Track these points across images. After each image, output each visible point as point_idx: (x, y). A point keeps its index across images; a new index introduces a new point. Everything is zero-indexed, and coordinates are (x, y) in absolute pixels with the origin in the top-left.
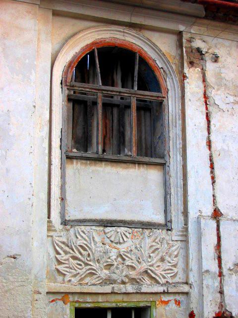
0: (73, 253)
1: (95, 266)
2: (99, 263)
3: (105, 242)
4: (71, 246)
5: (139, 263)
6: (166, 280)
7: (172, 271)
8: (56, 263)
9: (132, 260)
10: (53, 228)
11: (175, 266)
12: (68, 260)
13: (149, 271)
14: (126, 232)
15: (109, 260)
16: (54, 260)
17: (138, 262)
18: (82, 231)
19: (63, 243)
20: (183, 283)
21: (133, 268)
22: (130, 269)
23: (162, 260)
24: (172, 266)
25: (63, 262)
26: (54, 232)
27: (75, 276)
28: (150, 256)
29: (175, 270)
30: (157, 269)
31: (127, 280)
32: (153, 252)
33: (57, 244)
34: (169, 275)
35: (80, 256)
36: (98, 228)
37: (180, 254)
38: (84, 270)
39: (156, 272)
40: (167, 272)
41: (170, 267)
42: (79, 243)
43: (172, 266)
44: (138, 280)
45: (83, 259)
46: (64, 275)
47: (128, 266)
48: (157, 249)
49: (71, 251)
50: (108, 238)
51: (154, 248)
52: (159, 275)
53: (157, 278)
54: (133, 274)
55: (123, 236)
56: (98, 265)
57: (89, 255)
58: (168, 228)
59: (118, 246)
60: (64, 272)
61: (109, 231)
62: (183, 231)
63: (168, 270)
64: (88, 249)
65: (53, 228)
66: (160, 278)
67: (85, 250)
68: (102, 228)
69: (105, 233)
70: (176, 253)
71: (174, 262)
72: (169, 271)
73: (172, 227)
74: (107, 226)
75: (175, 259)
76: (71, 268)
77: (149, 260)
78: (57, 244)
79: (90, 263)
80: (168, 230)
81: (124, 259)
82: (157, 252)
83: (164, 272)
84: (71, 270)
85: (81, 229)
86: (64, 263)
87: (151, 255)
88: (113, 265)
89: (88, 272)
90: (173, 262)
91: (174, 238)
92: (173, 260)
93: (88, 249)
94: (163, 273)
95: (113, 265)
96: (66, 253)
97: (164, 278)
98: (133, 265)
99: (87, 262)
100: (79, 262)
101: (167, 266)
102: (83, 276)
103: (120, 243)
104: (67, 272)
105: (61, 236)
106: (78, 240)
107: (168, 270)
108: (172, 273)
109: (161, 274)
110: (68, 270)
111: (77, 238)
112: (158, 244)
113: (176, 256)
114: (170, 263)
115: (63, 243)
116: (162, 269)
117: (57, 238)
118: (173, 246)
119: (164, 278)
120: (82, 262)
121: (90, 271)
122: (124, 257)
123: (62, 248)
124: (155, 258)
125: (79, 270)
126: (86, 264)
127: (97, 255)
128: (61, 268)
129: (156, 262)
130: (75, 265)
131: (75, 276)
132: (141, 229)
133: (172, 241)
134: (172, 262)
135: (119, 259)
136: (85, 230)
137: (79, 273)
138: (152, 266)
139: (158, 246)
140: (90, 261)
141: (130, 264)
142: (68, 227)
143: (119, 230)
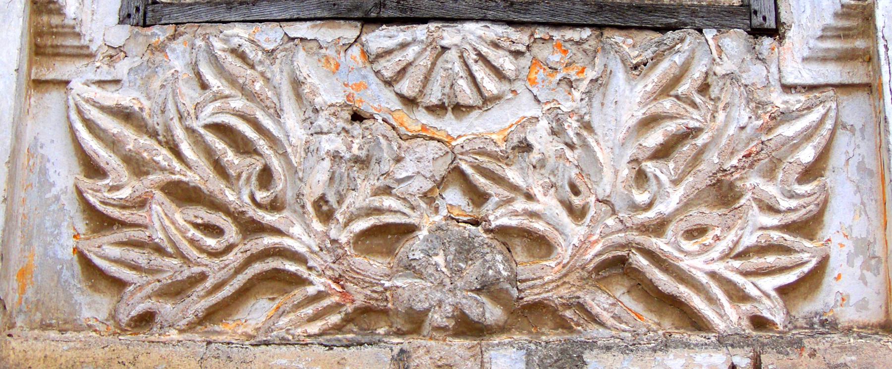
0: (177, 165)
1: (300, 234)
2: (327, 216)
3: (365, 107)
4: (168, 129)
5: (577, 214)
6: (746, 307)
7: (785, 260)
8: (82, 226)
9: (529, 197)
10: (71, 42)
11: (807, 227)
12: (142, 203)
13: (640, 261)
14: (496, 45)
15: (388, 202)
16: (72, 207)
17: (570, 209)
18: (233, 51)
19: (125, 115)
20: (439, 56)
21: (540, 244)
22: (520, 255)
23: (724, 193)
24: (786, 228)
25: (115, 213)
26: (80, 64)
27: (177, 291)
28: (641, 177)
29: (807, 253)
30: (689, 246)
31: (493, 313)
32: (663, 153)
33: (90, 124)
34: (770, 283)
35: (214, 185)
36: (327, 34)
37: (837, 159)
38: (234, 258)
39: (686, 264)
40: (756, 262)
41: (776, 235)
42: (208, 115)
43: (786, 228)
44: (568, 314)
45: (230, 196)
46: (119, 284)
47: (503, 232)
48: (690, 133)
49: (163, 156)
50: (389, 83)
51: (672, 127)
52: (704, 279)
53: (697, 302)
54: (542, 278)
55: (480, 72)
56: (317, 226)
57: (266, 177)
58: (757, 21)
59: (449, 125)
60: (114, 270)
61: (389, 44)
62: (844, 34)
63: (762, 250)
64: (262, 144)
65: (71, 42)
66: (711, 300)
67: (243, 146)
68: (349, 32)
69: (372, 58)
70: (807, 155)
71: (794, 207)
72: (771, 259)
73: (784, 17)
74: (380, 21)
75: (801, 189)
76: (159, 250)
77: (642, 198)
78: (90, 124)
79: (268, 218)
80: (757, 32)
81: (479, 197)
82: (686, 149)
83: (737, 264)
84: (158, 260)
85: (226, 40)
86: (123, 224)
87: (650, 167)
88: (408, 230)
89: (258, 267)
90: (793, 203)
91: (798, 72)
92: (792, 196)
93: (262, 144)
94: (729, 270)
95: (408, 230)
96: (138, 166)
97: (738, 295)
98: (539, 226)
99: (253, 212)
100: (205, 215)
101: (754, 226)
102: (227, 291)
103: (460, 109)
104: (136, 268)
105: (117, 82)
106: (208, 94)
107: (762, 250)
108: (783, 270)
109: (713, 275)
110: (134, 255)
111: (204, 86)
112: (694, 105)
113: (810, 172)
114: (771, 209)
115: (125, 115)
116: (723, 246)
117: (94, 92)
118: (785, 116)
119: (738, 295)
120: (228, 213)
121: (258, 267)
122: (480, 181)
123: (113, 143)
124: (676, 182)
125: (204, 258)
126: (252, 228)
127: (317, 180)
128: (106, 251)
129: (686, 205)
130: (183, 233)
131: (177, 291)
132: (586, 33)
133: (788, 88)
134: (784, 204)
135: (454, 197)
136: (248, 48)
137: (203, 277)
138: (659, 227)
139: (693, 119)
140: (275, 206)
141: (514, 222)
142: (159, 33)
143: (450, 35)
